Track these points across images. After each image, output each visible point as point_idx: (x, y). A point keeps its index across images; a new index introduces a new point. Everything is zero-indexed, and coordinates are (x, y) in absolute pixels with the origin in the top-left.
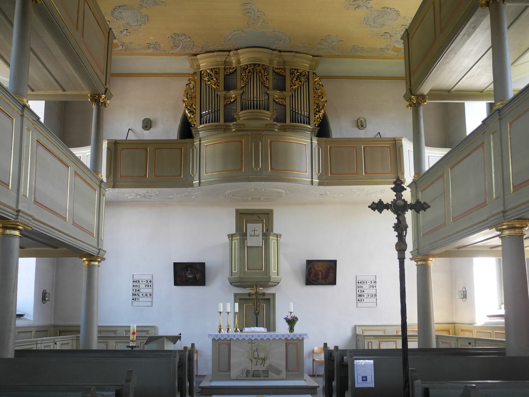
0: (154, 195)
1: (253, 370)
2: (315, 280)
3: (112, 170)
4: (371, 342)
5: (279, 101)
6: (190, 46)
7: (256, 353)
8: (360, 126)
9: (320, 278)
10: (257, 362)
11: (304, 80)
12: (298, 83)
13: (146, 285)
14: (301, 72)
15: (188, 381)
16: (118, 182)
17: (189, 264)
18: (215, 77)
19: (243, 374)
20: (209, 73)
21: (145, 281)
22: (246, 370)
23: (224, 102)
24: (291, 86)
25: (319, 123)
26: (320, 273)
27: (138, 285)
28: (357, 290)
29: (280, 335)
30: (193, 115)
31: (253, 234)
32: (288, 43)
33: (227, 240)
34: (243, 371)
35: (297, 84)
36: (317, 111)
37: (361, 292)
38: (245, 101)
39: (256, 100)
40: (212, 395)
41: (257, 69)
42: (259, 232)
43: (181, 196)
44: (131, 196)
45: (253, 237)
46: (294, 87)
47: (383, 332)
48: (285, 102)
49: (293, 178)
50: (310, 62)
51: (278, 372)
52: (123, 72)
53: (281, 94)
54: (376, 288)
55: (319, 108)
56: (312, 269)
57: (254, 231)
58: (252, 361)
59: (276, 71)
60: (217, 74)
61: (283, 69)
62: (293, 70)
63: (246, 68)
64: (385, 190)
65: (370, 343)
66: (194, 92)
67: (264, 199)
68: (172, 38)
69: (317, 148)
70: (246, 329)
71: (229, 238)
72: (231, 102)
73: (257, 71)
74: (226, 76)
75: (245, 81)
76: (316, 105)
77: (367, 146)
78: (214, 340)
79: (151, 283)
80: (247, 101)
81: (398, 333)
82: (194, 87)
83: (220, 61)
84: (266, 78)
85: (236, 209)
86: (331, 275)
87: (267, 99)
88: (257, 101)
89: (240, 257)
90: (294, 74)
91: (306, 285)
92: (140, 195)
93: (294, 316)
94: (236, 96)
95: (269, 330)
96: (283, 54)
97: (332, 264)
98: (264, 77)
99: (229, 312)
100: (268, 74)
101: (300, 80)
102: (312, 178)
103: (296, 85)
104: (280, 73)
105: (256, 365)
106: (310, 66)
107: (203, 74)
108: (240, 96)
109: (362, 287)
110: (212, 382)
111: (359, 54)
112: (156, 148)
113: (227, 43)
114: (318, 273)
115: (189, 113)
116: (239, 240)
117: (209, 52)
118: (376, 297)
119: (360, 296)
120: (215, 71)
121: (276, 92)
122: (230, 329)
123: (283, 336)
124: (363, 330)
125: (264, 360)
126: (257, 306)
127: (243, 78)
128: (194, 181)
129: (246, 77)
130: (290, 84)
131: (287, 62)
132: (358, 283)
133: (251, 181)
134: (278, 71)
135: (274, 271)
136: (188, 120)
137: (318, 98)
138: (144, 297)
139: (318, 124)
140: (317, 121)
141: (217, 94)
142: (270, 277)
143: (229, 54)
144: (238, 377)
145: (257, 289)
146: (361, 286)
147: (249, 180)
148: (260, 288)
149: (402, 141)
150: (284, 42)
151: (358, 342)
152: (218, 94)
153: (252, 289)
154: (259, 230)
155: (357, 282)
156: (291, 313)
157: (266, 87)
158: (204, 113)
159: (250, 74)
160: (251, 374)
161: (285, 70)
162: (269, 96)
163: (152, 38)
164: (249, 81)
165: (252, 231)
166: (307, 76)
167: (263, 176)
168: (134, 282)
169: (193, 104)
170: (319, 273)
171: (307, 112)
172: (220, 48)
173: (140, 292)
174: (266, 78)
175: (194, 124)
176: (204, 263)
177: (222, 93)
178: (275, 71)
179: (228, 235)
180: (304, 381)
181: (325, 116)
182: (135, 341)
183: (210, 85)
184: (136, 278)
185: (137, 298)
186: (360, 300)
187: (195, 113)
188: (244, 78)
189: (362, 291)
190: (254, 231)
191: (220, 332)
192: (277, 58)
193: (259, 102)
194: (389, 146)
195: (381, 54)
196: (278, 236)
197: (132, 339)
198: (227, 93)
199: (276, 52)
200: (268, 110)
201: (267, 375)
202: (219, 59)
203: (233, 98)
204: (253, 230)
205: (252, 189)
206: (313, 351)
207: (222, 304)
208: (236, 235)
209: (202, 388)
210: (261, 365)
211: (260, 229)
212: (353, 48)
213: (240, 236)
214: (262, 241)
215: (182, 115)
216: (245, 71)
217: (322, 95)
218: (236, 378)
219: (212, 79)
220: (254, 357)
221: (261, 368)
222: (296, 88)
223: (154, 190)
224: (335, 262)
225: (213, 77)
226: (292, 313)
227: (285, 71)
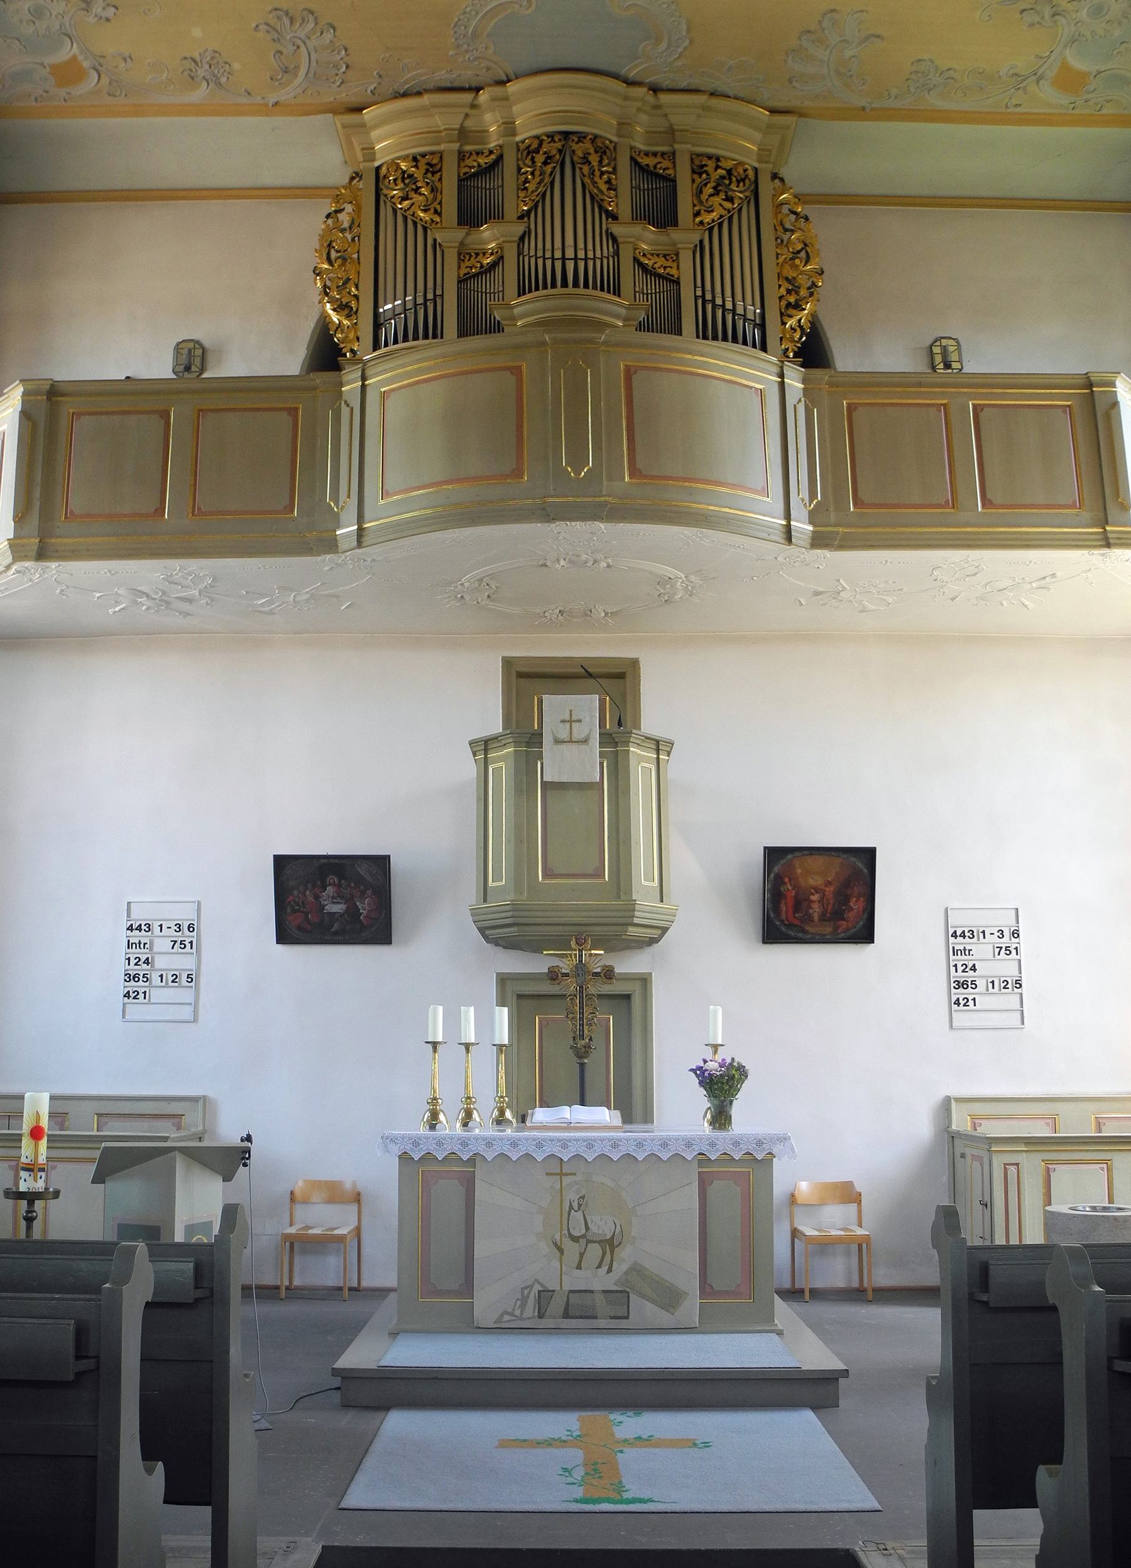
0: (196, 592)
1: (567, 1287)
2: (797, 922)
3: (37, 493)
4: (1017, 1164)
5: (655, 266)
6: (336, 66)
7: (580, 1214)
8: (941, 366)
9: (816, 917)
10: (582, 1255)
11: (741, 195)
12: (720, 205)
13: (175, 942)
14: (731, 169)
15: (149, 1454)
16: (58, 537)
17: (332, 861)
18: (428, 184)
19: (523, 1306)
20: (404, 172)
21: (172, 924)
22: (537, 1288)
23: (459, 267)
24: (697, 214)
25: (799, 345)
26: (815, 897)
27: (147, 940)
28: (952, 964)
29: (677, 1140)
30: (348, 316)
31: (564, 734)
32: (685, 48)
33: (469, 769)
34: (526, 1292)
35: (716, 205)
36: (789, 305)
37: (963, 971)
38: (533, 261)
39: (573, 257)
40: (387, 1408)
41: (573, 151)
42: (590, 726)
43: (298, 599)
44: (117, 603)
45: (564, 747)
46: (707, 218)
47: (1047, 1124)
48: (678, 268)
49: (717, 509)
50: (758, 136)
51: (670, 1298)
52: (116, 188)
53: (663, 238)
54: (1018, 957)
55: (797, 293)
56: (787, 880)
57: (571, 721)
58: (561, 1251)
59: (644, 161)
60: (433, 173)
61: (666, 157)
62: (701, 158)
63: (535, 145)
64: (1053, 575)
65: (1013, 1168)
66: (353, 240)
67: (606, 614)
68: (268, 32)
69: (801, 408)
70: (541, 1115)
71: (475, 754)
72: (482, 266)
73: (575, 159)
74: (463, 182)
75: (533, 192)
76: (786, 285)
77: (984, 405)
78: (404, 1158)
79: (194, 934)
80: (540, 261)
81: (1103, 1128)
82: (353, 223)
83: (443, 128)
84: (606, 182)
85: (503, 658)
86: (857, 905)
87: (611, 253)
88: (576, 259)
89: (518, 828)
90: (706, 172)
91: (764, 942)
92: (148, 596)
93: (733, 1059)
94: (500, 247)
95: (627, 1119)
96: (665, 98)
97: (860, 865)
98: (601, 178)
99: (473, 1044)
100: (614, 169)
101: (726, 192)
102: (788, 516)
103: (712, 211)
104: (655, 167)
105: (579, 1267)
106: (759, 149)
107: (385, 177)
108: (516, 245)
109: (970, 950)
110: (399, 1337)
111: (935, 101)
112: (201, 410)
113: (467, 51)
114: (807, 899)
115: (334, 310)
116: (512, 763)
117: (405, 95)
118: (1019, 990)
119: (961, 985)
120: (428, 164)
121: (645, 229)
122: (475, 1115)
123: (689, 1144)
124: (973, 1118)
125: (610, 1245)
126: (581, 1019)
127: (526, 181)
128: (339, 527)
129: (538, 179)
130: (694, 206)
131: (680, 131)
132: (955, 935)
133: (554, 520)
134: (650, 161)
135: (647, 883)
136: (332, 337)
137: (792, 259)
138: (167, 986)
139: (796, 349)
140: (792, 340)
141: (435, 240)
142: (631, 907)
143: (475, 103)
144: (506, 1318)
145: (581, 951)
146: (965, 950)
147: (548, 514)
148: (593, 952)
149: (1115, 387)
150: (669, 46)
151: (959, 1162)
152: (439, 240)
153: (561, 956)
154: (588, 718)
155: (951, 931)
156: (715, 1047)
157: (607, 211)
158: (386, 307)
159: (549, 169)
160: (557, 1305)
161: (674, 158)
162: (618, 247)
163: (197, 32)
164: (545, 191)
165: (563, 721)
166: (750, 185)
167: (602, 499)
168: (130, 928)
169: (348, 280)
170: (813, 898)
171: (753, 305)
172: (443, 76)
173: (153, 969)
174: (609, 182)
175: (352, 351)
176: (387, 858)
177: (450, 235)
178: (640, 160)
179: (471, 743)
180: (774, 1336)
181: (815, 323)
182: (43, 1170)
183: (411, 212)
184: (140, 915)
185: (141, 990)
186: (961, 1001)
187: (357, 310)
188: (529, 182)
189: (970, 966)
190: (571, 721)
191: (433, 1127)
192: (644, 118)
193: (581, 264)
194: (1069, 406)
195: (1014, 102)
196: (658, 745)
197: (28, 1161)
198: (468, 234)
199: (641, 91)
200: (617, 292)
201: (622, 1311)
202: (439, 121)
203: (492, 254)
204: (567, 717)
205: (562, 563)
206: (793, 1195)
207: (441, 1008)
208: (499, 741)
209: (349, 1377)
210: (599, 1266)
211: (592, 717)
212: (916, 72)
213: (516, 743)
214: (601, 764)
215: (312, 325)
216: (533, 159)
217: (807, 253)
218: (495, 1323)
219: (417, 190)
220: (570, 1236)
221: (601, 1281)
222: (713, 221)
223: (193, 565)
224: (869, 854)
225: (419, 184)
226: (720, 1048)
227: (674, 163)
